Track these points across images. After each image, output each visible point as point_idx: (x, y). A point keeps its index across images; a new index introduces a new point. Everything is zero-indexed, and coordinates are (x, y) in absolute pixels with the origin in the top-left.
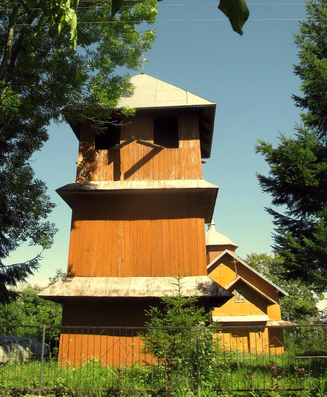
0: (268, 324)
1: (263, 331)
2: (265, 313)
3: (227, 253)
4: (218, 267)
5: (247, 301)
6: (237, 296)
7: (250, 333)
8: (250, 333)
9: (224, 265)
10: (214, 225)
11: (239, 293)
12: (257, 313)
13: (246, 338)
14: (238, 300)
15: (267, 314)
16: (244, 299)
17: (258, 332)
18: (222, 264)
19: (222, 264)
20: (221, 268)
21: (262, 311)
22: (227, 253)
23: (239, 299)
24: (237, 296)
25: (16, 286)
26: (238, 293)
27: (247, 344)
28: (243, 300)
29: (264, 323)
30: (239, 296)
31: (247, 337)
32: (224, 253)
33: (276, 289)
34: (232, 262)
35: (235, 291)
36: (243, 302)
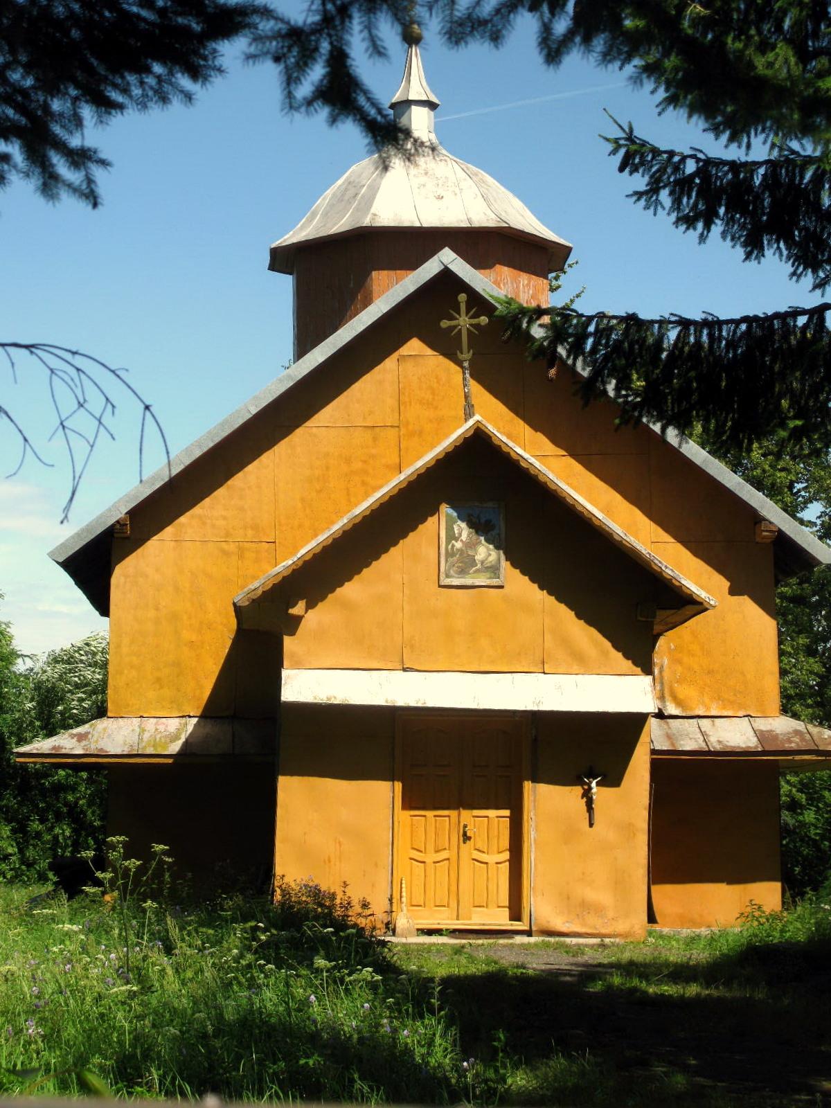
0: (655, 736)
1: (613, 778)
2: (636, 664)
3: (446, 275)
4: (390, 363)
5: (519, 584)
6: (458, 545)
7: (528, 786)
8: (528, 786)
9: (429, 352)
10: (432, 106)
11: (471, 525)
12: (581, 663)
13: (498, 818)
14: (463, 572)
15: (647, 669)
16: (505, 565)
17: (582, 783)
18: (414, 346)
19: (414, 346)
20: (409, 366)
21: (617, 647)
22: (446, 275)
23: (466, 563)
24: (458, 545)
25: (58, 563)
26: (463, 525)
27: (506, 855)
28: (494, 570)
29: (631, 724)
30: (471, 545)
31: (507, 813)
32: (430, 269)
33: (755, 518)
34: (445, 324)
35: (450, 511)
36: (495, 582)
